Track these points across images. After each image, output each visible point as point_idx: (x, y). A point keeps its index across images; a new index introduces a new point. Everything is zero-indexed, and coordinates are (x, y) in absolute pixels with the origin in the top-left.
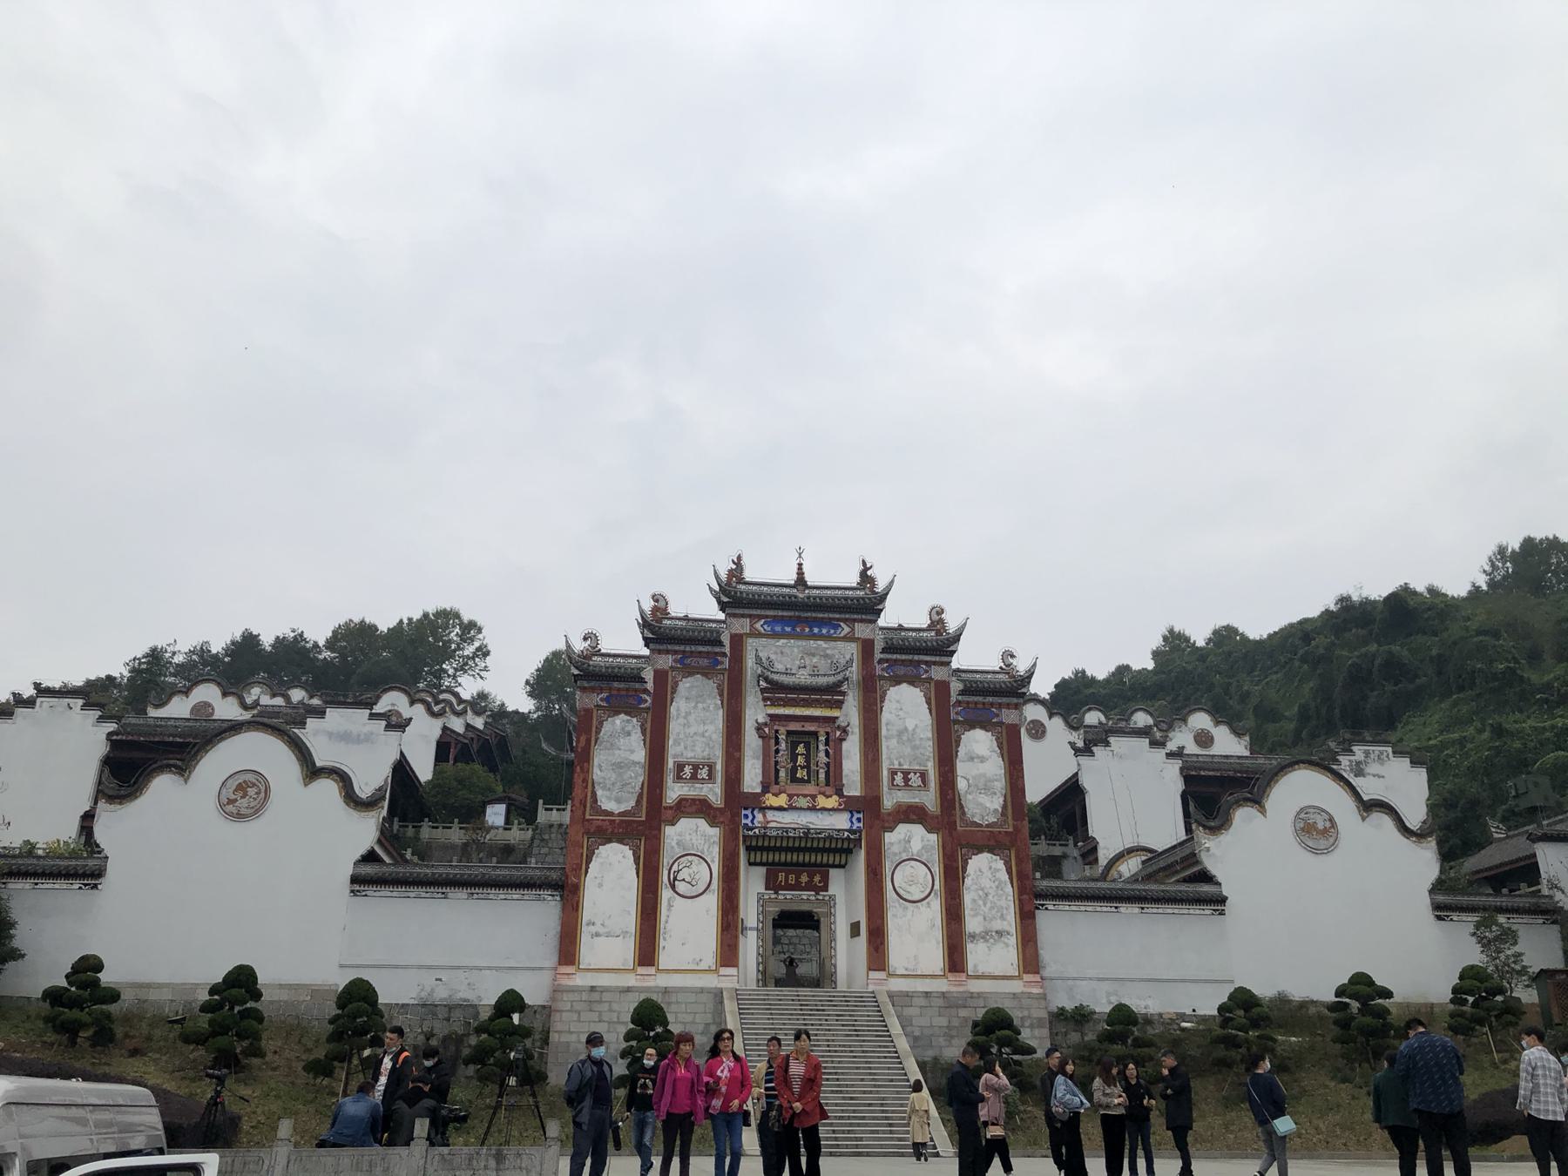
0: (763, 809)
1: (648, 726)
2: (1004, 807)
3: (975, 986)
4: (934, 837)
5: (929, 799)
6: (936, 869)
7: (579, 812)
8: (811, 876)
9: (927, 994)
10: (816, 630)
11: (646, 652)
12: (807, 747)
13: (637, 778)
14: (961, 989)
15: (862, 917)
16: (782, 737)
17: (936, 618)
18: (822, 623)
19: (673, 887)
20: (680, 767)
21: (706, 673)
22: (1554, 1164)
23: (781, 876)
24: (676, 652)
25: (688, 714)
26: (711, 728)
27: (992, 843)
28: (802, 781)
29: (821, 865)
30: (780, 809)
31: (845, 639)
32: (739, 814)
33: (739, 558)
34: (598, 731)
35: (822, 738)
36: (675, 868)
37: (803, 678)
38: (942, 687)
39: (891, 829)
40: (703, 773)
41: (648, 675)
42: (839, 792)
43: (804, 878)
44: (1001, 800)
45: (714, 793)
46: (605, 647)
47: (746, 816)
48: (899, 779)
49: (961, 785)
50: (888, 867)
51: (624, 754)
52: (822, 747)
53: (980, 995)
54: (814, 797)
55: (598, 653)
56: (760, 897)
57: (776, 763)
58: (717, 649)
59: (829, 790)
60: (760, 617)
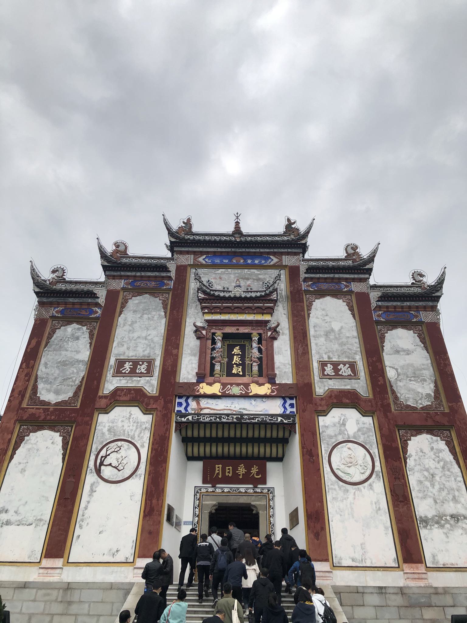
0: (198, 397)
1: (96, 332)
2: (437, 391)
3: (439, 580)
4: (368, 420)
5: (361, 385)
6: (375, 451)
7: (17, 402)
8: (248, 468)
9: (381, 590)
10: (249, 261)
11: (103, 278)
12: (243, 348)
13: (79, 373)
14: (422, 584)
15: (299, 503)
16: (218, 338)
17: (351, 251)
18: (254, 256)
19: (98, 471)
20: (120, 363)
21: (153, 292)
22: (189, 564)
23: (218, 468)
24: (128, 277)
25: (133, 323)
26: (153, 333)
27: (430, 422)
28: (237, 375)
29: (258, 458)
30: (213, 396)
31: (274, 267)
32: (171, 402)
33: (189, 220)
34: (50, 337)
35: (256, 338)
36: (103, 453)
37: (238, 292)
38: (363, 298)
39: (325, 413)
40: (142, 368)
41: (102, 294)
42: (272, 380)
43: (242, 470)
44: (432, 386)
45: (151, 385)
46: (69, 277)
47: (180, 404)
48: (329, 369)
49: (391, 374)
50: (324, 449)
51: (69, 354)
52: (255, 345)
53: (446, 591)
54: (247, 386)
55: (64, 281)
56: (197, 490)
57: (213, 358)
58: (164, 274)
59: (261, 380)
60: (202, 253)
